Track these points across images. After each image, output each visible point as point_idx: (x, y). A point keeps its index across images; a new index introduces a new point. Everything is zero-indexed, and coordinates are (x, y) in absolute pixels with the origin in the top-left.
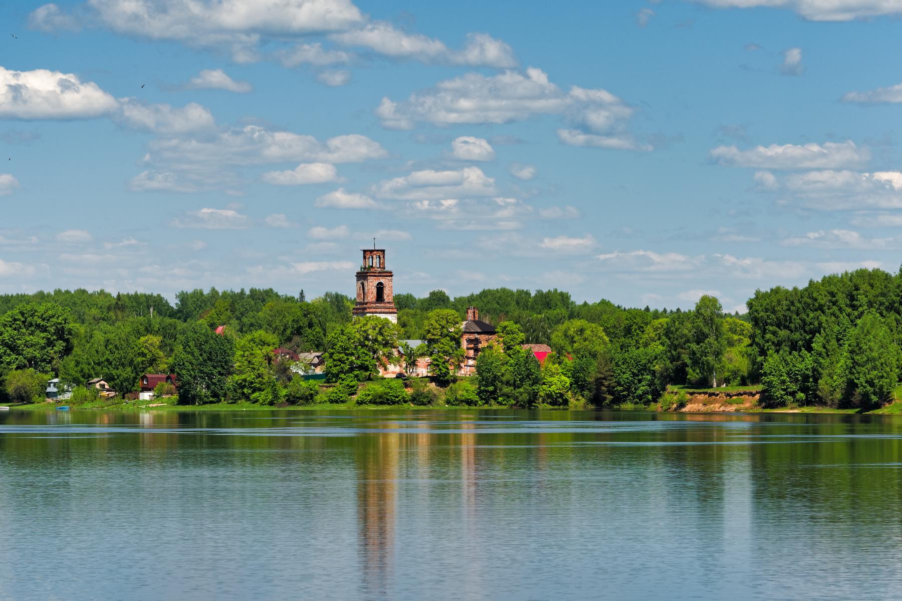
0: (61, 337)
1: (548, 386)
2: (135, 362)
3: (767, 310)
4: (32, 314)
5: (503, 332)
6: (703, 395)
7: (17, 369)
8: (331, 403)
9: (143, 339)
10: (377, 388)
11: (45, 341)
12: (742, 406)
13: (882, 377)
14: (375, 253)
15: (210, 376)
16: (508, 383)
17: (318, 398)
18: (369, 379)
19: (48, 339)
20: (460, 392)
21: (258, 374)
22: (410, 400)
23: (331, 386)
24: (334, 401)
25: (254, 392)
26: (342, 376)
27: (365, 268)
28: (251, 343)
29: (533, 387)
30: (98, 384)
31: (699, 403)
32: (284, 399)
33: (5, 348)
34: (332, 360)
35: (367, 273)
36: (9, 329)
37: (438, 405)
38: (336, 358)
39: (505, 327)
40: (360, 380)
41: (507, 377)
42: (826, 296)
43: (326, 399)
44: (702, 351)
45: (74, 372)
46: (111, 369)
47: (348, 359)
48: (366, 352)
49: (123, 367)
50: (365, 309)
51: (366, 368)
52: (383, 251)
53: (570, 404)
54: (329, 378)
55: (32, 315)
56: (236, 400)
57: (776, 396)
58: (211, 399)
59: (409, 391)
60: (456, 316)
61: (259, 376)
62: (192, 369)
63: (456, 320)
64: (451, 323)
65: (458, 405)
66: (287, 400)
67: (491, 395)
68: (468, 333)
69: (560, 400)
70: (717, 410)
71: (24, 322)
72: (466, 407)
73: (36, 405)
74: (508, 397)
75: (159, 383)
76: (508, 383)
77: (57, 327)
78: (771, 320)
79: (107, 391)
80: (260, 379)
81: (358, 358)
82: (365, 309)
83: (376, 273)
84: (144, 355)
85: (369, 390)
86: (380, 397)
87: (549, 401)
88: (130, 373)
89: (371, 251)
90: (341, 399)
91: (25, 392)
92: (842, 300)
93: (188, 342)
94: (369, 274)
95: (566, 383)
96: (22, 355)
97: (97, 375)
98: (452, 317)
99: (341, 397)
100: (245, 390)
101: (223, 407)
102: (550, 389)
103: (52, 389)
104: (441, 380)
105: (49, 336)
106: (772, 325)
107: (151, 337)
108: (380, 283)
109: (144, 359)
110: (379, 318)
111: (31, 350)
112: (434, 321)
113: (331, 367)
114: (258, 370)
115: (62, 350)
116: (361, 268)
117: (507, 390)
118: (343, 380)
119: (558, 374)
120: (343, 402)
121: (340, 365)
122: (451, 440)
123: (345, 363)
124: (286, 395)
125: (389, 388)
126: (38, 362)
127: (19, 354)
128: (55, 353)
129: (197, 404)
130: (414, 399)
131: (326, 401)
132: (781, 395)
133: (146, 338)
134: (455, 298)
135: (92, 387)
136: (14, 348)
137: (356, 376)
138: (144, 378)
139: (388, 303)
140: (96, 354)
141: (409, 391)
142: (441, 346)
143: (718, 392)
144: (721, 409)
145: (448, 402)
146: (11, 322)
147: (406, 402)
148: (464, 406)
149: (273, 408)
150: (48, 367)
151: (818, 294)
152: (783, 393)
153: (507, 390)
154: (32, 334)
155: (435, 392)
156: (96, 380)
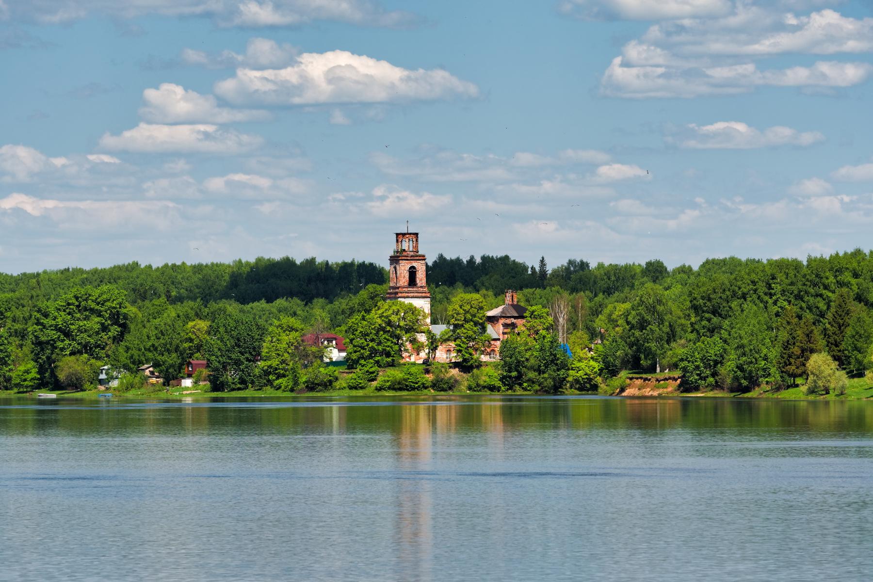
0: (116, 323)
1: (576, 371)
2: (181, 348)
3: (703, 298)
4: (87, 298)
5: (530, 317)
6: (640, 380)
7: (71, 354)
8: (350, 389)
9: (191, 324)
10: (396, 374)
11: (98, 326)
12: (665, 390)
13: (751, 362)
14: (407, 236)
15: (238, 363)
16: (532, 368)
17: (337, 384)
18: (392, 365)
19: (102, 324)
20: (483, 378)
21: (282, 360)
22: (431, 386)
23: (352, 372)
24: (353, 388)
25: (277, 378)
26: (362, 362)
27: (397, 252)
28: (279, 329)
29: (559, 373)
30: (147, 371)
31: (636, 388)
32: (303, 386)
33: (59, 333)
34: (352, 346)
35: (399, 256)
36: (62, 313)
37: (460, 391)
38: (355, 344)
39: (533, 312)
40: (381, 366)
41: (532, 361)
42: (748, 285)
43: (345, 385)
44: (645, 338)
45: (123, 357)
46: (156, 355)
47: (368, 345)
48: (387, 337)
49: (169, 353)
50: (397, 293)
51: (388, 355)
52: (416, 234)
53: (599, 390)
54: (350, 364)
55: (86, 300)
56: (262, 386)
57: (691, 381)
58: (239, 386)
59: (430, 377)
60: (481, 300)
61: (283, 362)
62: (221, 356)
63: (480, 304)
64: (475, 308)
65: (480, 390)
66: (307, 387)
67: (515, 381)
68: (504, 317)
69: (588, 385)
70: (647, 394)
71: (78, 306)
72: (489, 392)
73: (87, 392)
74: (533, 382)
75: (197, 369)
76: (532, 368)
77: (111, 311)
78: (707, 308)
79: (156, 378)
80: (284, 365)
81: (379, 344)
82: (397, 293)
83: (408, 256)
84: (191, 340)
85: (388, 376)
86: (399, 383)
87: (577, 386)
88: (175, 360)
89: (404, 235)
90: (360, 385)
91: (77, 379)
92: (762, 288)
93: (218, 327)
94: (400, 258)
95: (594, 368)
96: (75, 340)
97: (147, 361)
98: (475, 302)
99: (360, 383)
100: (271, 377)
101: (249, 393)
102: (577, 374)
103: (103, 376)
104: (465, 366)
105: (103, 321)
106: (708, 313)
107: (199, 322)
108: (413, 267)
109: (191, 344)
110: (404, 303)
111: (85, 335)
112: (458, 306)
113: (351, 353)
114: (283, 356)
115: (117, 335)
116: (394, 252)
117: (532, 375)
118: (363, 366)
119: (587, 359)
120: (362, 388)
121: (360, 351)
122: (205, 416)
123: (365, 349)
124: (306, 382)
125: (409, 374)
126: (92, 348)
127: (73, 340)
128: (109, 338)
129: (226, 391)
130: (435, 385)
131: (345, 388)
132: (696, 379)
133: (194, 323)
134: (768, 260)
135: (140, 373)
136: (67, 334)
137: (377, 362)
138: (189, 364)
139: (421, 287)
140: (147, 340)
141: (430, 377)
142: (465, 331)
143: (650, 377)
144: (650, 394)
145: (470, 388)
146: (65, 306)
147: (426, 388)
148: (486, 392)
149: (293, 394)
150: (102, 353)
151: (741, 282)
152: (697, 377)
153: (532, 375)
154: (87, 318)
155: (458, 378)
156: (146, 366)
